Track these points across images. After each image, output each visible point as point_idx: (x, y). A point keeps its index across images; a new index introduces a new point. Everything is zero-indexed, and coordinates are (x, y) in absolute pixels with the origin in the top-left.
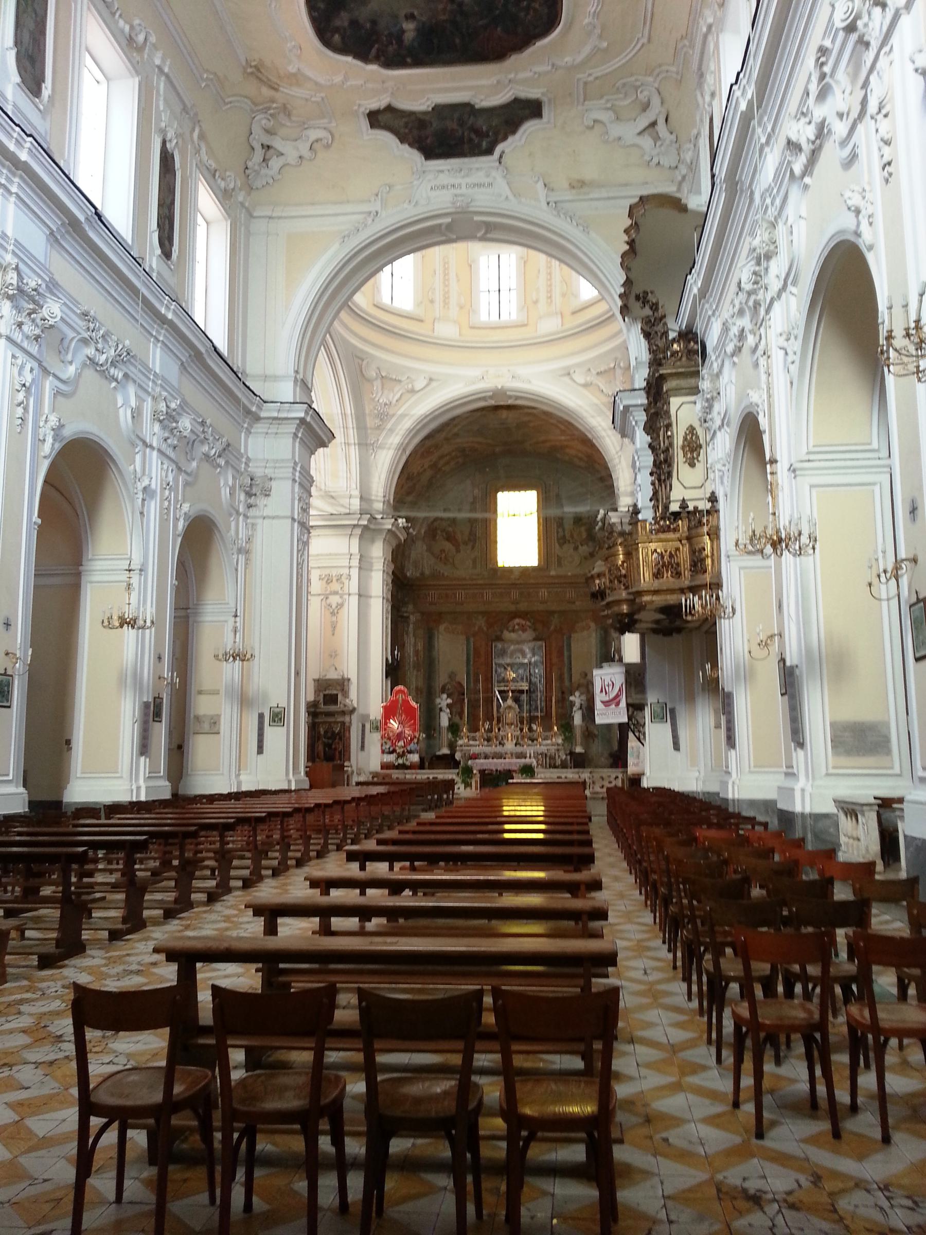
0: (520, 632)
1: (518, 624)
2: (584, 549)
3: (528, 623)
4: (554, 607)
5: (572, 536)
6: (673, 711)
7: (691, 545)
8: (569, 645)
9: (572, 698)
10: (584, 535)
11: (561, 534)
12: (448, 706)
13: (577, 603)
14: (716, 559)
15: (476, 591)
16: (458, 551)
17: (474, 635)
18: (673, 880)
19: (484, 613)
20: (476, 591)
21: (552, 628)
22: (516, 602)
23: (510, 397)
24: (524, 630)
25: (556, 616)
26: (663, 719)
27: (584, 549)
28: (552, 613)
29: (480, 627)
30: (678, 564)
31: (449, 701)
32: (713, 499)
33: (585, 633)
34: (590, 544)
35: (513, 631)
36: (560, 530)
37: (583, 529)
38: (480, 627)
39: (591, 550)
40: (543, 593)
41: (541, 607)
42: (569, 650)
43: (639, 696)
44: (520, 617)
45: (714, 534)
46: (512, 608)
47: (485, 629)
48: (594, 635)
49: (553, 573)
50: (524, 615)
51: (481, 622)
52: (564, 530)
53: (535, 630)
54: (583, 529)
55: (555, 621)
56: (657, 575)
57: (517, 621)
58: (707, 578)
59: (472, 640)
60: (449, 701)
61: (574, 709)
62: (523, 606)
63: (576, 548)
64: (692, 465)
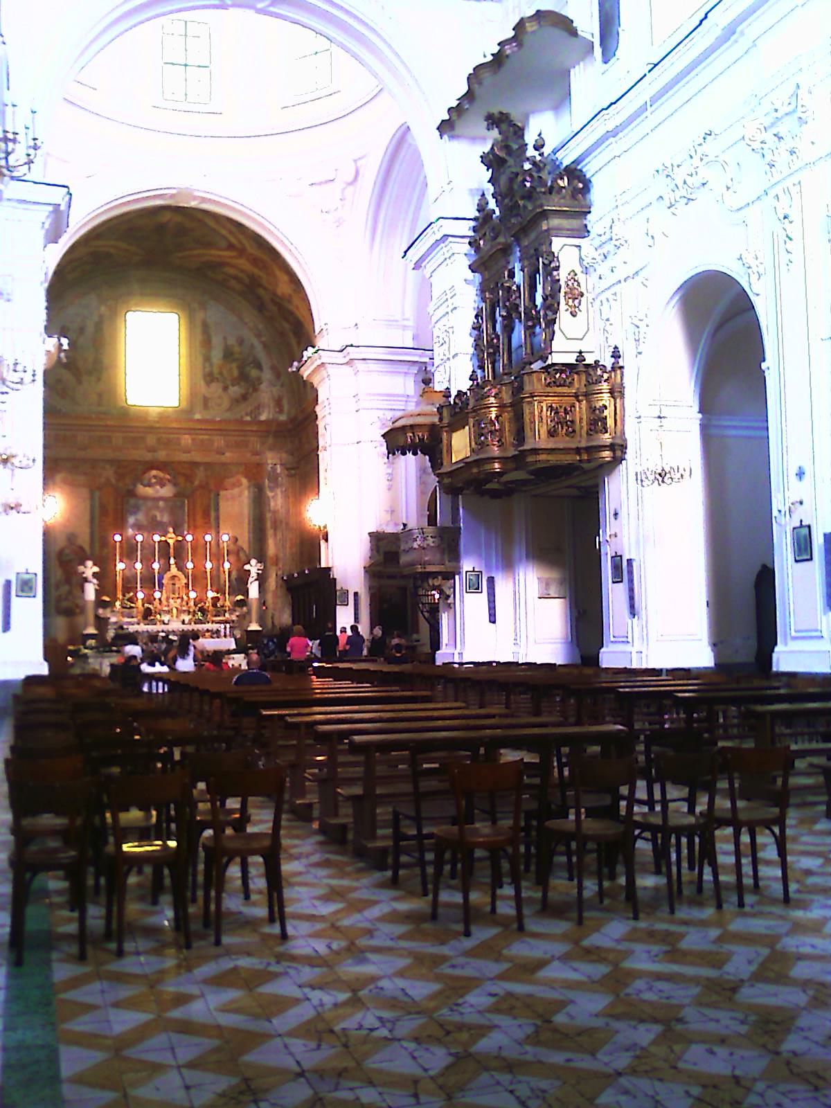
0: (158, 487)
1: (155, 477)
2: (235, 390)
3: (168, 477)
4: (197, 457)
5: (221, 373)
6: (491, 581)
7: (589, 402)
8: (217, 505)
9: (247, 567)
10: (236, 373)
11: (207, 370)
12: (95, 575)
13: (228, 454)
14: (619, 418)
15: (103, 434)
16: (79, 382)
17: (99, 488)
18: (164, 825)
19: (112, 462)
20: (103, 434)
21: (197, 483)
22: (152, 450)
23: (195, 198)
24: (162, 485)
25: (202, 468)
26: (477, 589)
27: (235, 390)
28: (195, 464)
29: (108, 479)
30: (572, 422)
31: (96, 569)
32: (616, 355)
33: (236, 491)
34: (242, 383)
35: (149, 485)
36: (207, 365)
37: (234, 365)
38: (108, 479)
39: (243, 391)
40: (186, 440)
41: (185, 457)
42: (217, 510)
43: (454, 564)
44: (157, 469)
45: (617, 392)
46: (149, 456)
47: (113, 481)
48: (246, 493)
49: (198, 416)
50: (161, 466)
51: (109, 473)
52: (211, 365)
53: (175, 485)
54: (234, 365)
55: (200, 475)
56: (552, 434)
57: (154, 472)
58: (606, 438)
59: (97, 494)
60: (96, 569)
61: (251, 580)
62: (162, 455)
63: (225, 388)
64: (574, 315)
